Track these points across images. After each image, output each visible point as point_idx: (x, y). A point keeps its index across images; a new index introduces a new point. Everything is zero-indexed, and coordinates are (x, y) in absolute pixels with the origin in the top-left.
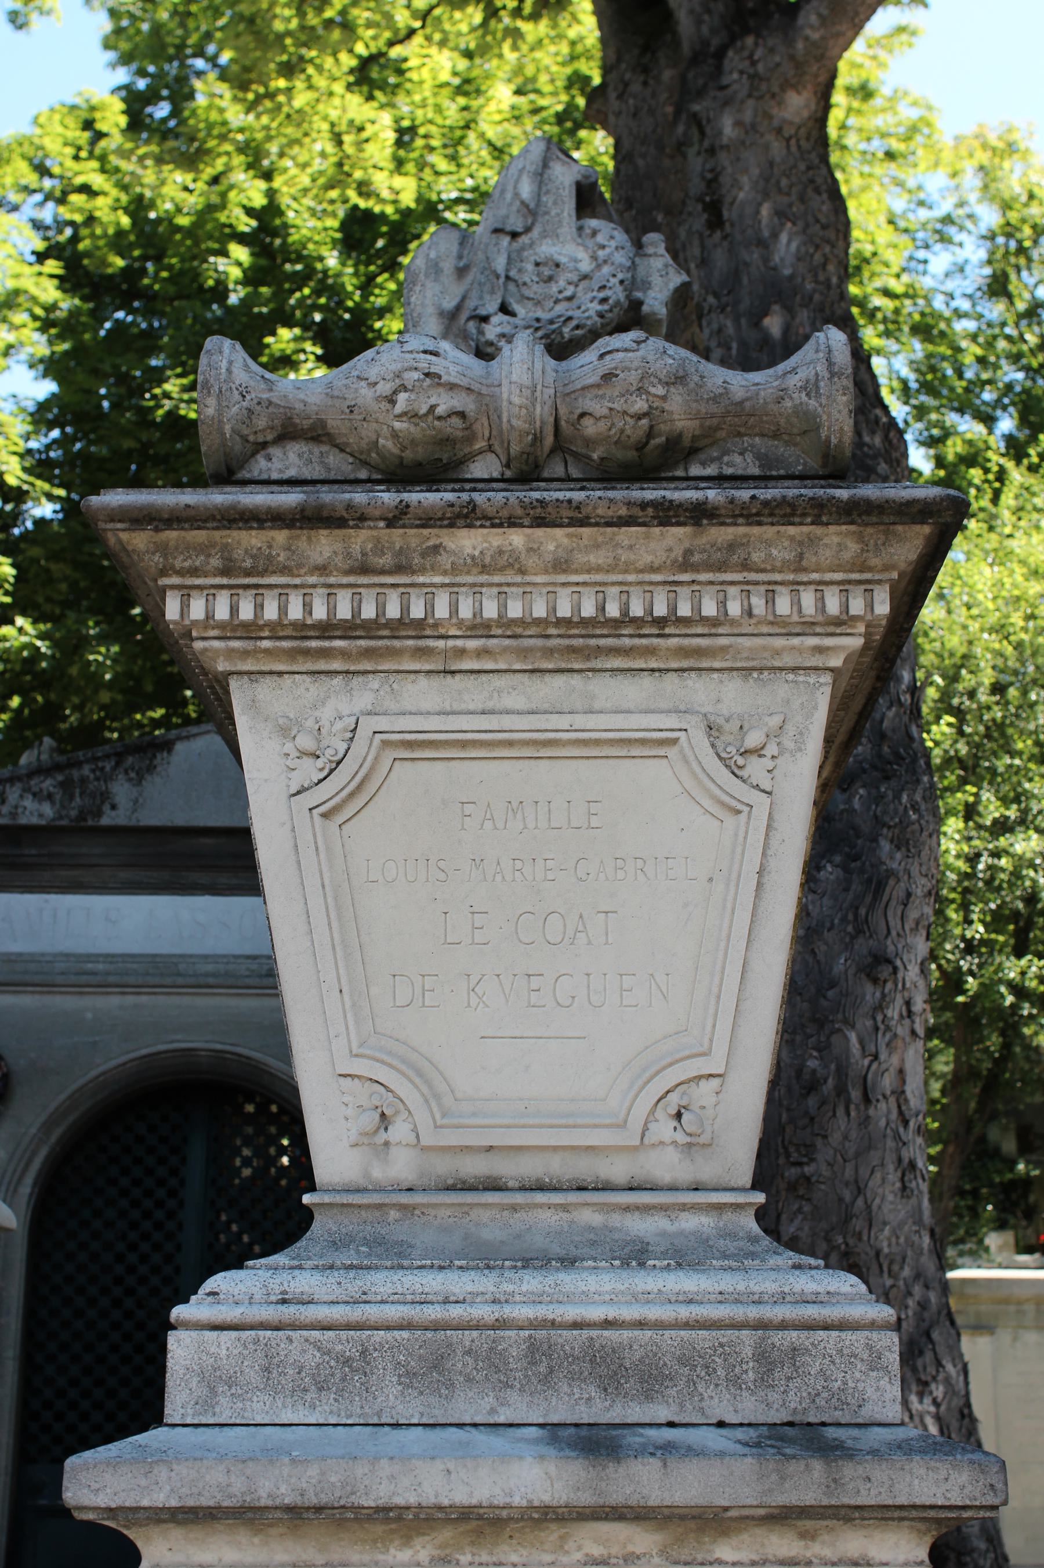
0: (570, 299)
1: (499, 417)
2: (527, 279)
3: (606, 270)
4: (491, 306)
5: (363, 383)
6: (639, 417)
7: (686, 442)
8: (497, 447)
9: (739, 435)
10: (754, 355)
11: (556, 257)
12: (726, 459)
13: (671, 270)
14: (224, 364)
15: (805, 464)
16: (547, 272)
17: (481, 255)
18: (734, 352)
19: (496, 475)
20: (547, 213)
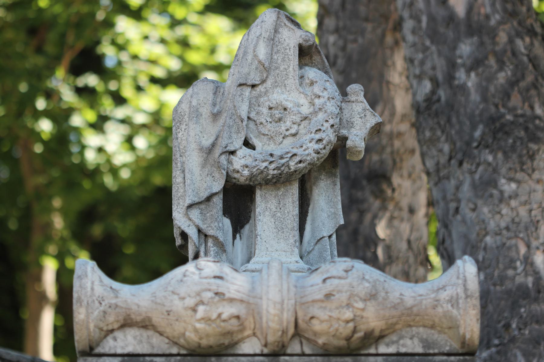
0: (294, 135)
1: (261, 318)
2: (264, 121)
3: (321, 116)
4: (238, 143)
5: (176, 297)
6: (348, 322)
7: (377, 333)
8: (258, 334)
9: (410, 326)
10: (442, 30)
11: (284, 103)
12: (401, 342)
13: (368, 114)
14: (89, 285)
15: (451, 346)
16: (277, 114)
17: (229, 104)
18: (424, 24)
19: (258, 351)
20: (277, 68)
